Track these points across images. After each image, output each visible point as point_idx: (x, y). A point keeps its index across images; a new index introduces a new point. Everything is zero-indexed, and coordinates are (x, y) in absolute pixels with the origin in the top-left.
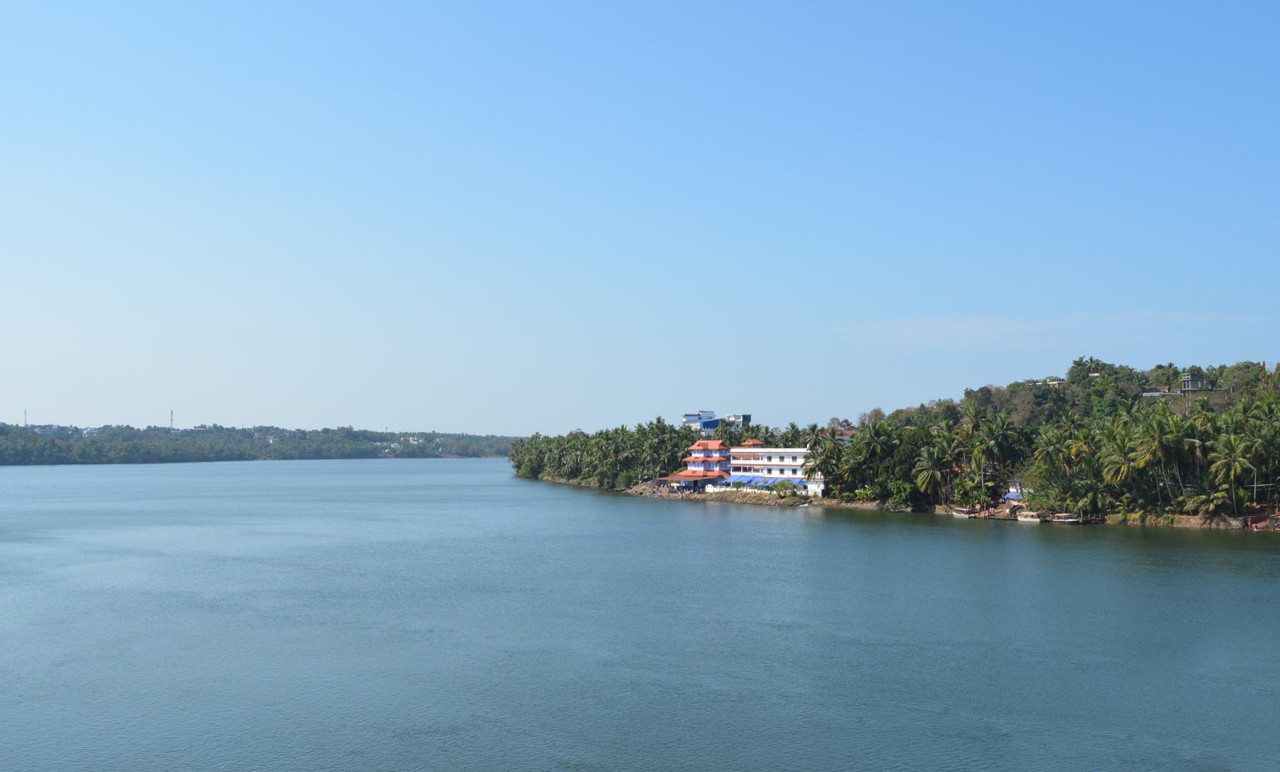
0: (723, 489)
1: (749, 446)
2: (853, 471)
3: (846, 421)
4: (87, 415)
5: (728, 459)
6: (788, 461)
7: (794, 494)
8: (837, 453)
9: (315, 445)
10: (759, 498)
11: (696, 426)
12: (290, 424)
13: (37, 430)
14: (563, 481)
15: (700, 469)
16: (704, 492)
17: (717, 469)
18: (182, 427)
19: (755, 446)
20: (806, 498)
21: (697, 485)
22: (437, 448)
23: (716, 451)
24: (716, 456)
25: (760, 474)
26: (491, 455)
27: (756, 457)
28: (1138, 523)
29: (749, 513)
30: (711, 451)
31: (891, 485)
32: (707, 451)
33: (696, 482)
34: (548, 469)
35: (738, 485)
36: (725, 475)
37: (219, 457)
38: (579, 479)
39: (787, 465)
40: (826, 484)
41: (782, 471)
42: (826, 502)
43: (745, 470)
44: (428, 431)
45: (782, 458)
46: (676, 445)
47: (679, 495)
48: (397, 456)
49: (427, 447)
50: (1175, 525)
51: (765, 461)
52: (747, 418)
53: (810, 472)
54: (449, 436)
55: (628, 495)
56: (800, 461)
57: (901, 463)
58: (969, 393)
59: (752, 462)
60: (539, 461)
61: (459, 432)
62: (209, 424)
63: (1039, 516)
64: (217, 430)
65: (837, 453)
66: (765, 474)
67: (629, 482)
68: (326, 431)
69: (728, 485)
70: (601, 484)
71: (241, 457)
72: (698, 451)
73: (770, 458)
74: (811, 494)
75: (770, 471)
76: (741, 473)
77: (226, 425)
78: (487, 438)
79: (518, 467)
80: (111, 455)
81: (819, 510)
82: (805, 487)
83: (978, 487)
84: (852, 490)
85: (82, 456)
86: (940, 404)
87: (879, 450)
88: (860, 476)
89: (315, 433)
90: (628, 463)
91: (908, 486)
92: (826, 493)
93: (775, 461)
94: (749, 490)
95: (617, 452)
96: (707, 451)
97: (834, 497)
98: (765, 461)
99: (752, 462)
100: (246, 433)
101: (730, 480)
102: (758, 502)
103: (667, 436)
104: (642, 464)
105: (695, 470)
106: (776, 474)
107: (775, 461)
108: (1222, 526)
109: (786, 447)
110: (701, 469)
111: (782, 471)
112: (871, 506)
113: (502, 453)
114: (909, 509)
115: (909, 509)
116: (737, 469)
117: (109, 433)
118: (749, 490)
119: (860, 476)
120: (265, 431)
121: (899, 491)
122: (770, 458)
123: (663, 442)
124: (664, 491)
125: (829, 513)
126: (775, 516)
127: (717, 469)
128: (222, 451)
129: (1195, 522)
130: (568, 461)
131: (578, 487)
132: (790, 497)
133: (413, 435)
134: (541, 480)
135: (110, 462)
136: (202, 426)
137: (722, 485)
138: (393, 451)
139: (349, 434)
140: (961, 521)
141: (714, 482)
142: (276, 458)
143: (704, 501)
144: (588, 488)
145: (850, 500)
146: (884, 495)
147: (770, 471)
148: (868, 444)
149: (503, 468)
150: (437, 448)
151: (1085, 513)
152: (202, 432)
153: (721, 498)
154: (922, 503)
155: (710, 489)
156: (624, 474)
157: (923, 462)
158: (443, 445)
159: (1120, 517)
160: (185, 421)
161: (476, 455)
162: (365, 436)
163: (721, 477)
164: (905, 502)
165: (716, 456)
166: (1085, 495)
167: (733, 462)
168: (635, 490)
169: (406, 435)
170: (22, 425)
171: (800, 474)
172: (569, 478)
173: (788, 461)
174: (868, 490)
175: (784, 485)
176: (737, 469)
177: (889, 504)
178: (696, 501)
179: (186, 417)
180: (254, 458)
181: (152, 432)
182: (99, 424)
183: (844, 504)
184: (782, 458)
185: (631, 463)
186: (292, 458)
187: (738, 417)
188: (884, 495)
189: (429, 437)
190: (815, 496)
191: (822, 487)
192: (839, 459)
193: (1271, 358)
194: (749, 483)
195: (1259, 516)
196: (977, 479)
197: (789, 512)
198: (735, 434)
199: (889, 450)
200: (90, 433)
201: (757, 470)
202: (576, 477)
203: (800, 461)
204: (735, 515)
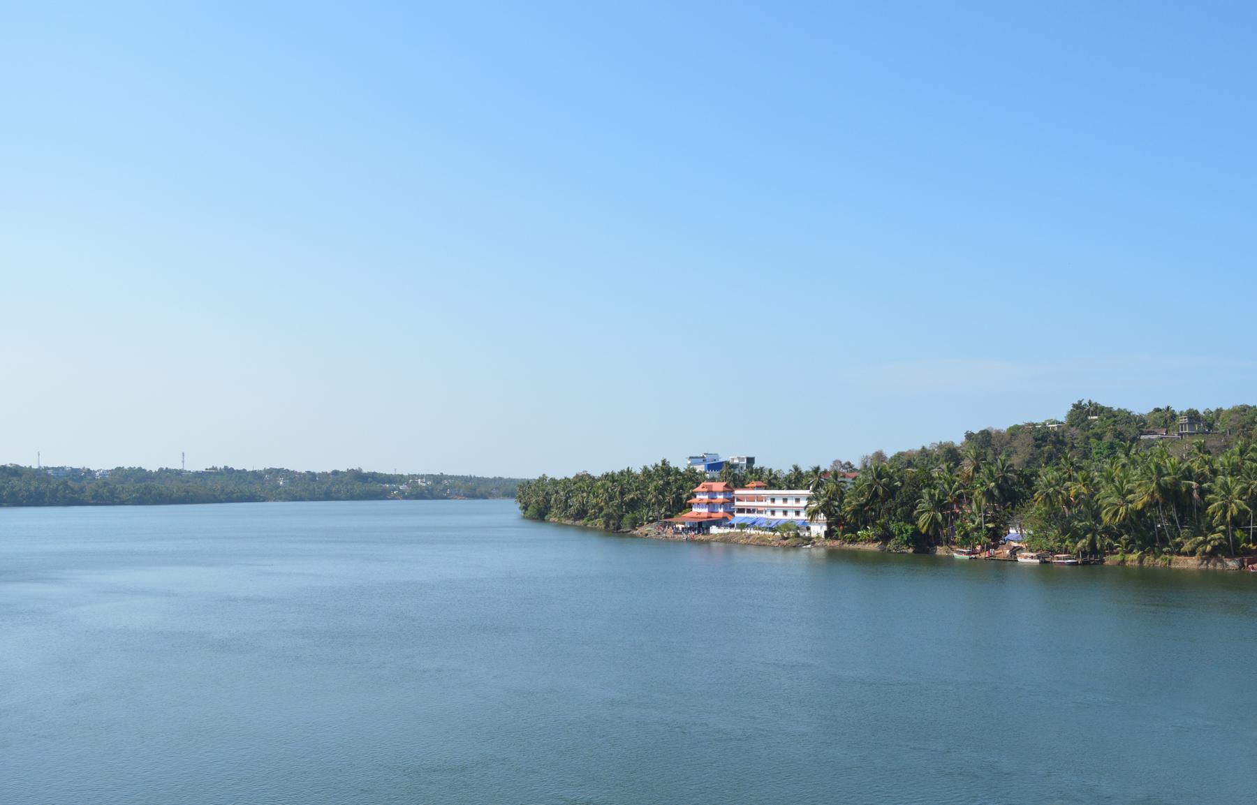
0: (727, 530)
1: (753, 488)
2: (855, 512)
3: (849, 463)
4: (100, 457)
5: (732, 501)
6: (791, 503)
7: (797, 535)
8: (839, 495)
10: (762, 539)
11: (700, 468)
12: (300, 464)
13: (50, 472)
14: (569, 522)
15: (705, 511)
16: (708, 533)
17: (721, 510)
19: (758, 487)
20: (810, 539)
21: (701, 526)
22: (445, 490)
23: (720, 493)
24: (720, 497)
25: (763, 515)
26: (498, 496)
27: (760, 499)
28: (1136, 564)
29: (753, 554)
31: (893, 527)
33: (700, 524)
34: (554, 510)
35: (742, 526)
36: (729, 516)
38: (585, 520)
39: (791, 506)
40: (829, 525)
41: (785, 513)
42: (829, 543)
43: (749, 511)
44: (436, 472)
45: (785, 500)
46: (681, 487)
47: (684, 537)
48: (406, 498)
49: (436, 489)
50: (1173, 566)
51: (769, 503)
52: (751, 461)
53: (813, 514)
54: (457, 478)
55: (633, 536)
56: (804, 503)
57: (902, 504)
58: (969, 436)
59: (756, 504)
60: (545, 502)
61: (466, 474)
62: (220, 466)
63: (1038, 557)
64: (228, 471)
65: (839, 495)
66: (768, 515)
67: (635, 524)
68: (335, 473)
69: (732, 526)
70: (607, 525)
71: (251, 498)
73: (773, 500)
75: (773, 512)
76: (745, 515)
78: (495, 480)
79: (525, 508)
80: (124, 496)
81: (822, 551)
82: (808, 529)
83: (978, 529)
84: (854, 532)
86: (941, 446)
87: (881, 491)
88: (862, 517)
89: (325, 475)
90: (633, 505)
91: (909, 527)
92: (829, 534)
93: (779, 503)
94: (753, 532)
95: (622, 494)
97: (837, 539)
101: (734, 521)
102: (762, 544)
103: (672, 478)
104: (648, 506)
105: (700, 512)
106: (779, 515)
107: (779, 503)
108: (1219, 566)
109: (789, 488)
110: (706, 510)
111: (785, 513)
112: (874, 547)
113: (509, 495)
114: (911, 550)
115: (911, 550)
116: (741, 510)
118: (753, 532)
119: (862, 517)
121: (901, 532)
122: (773, 500)
123: (668, 483)
124: (669, 532)
125: (832, 554)
126: (779, 557)
127: (721, 510)
128: (232, 493)
129: (1192, 563)
130: (575, 502)
131: (584, 529)
132: (794, 538)
133: (422, 477)
134: (548, 521)
135: (122, 503)
136: (214, 468)
139: (358, 476)
140: (962, 562)
141: (718, 523)
142: (286, 500)
143: (708, 542)
144: (594, 530)
145: (853, 541)
146: (886, 537)
147: (773, 512)
148: (870, 486)
149: (511, 509)
150: (445, 490)
151: (1084, 554)
152: (212, 474)
153: (726, 539)
154: (924, 544)
155: (714, 530)
156: (630, 515)
157: (924, 504)
158: (452, 487)
159: (1118, 558)
160: (196, 463)
161: (484, 496)
162: (373, 477)
163: (725, 519)
164: (907, 543)
165: (720, 497)
166: (1084, 537)
167: (737, 503)
168: (639, 531)
169: (414, 477)
170: (35, 467)
171: (803, 516)
172: (575, 520)
173: (791, 503)
174: (870, 532)
175: (787, 526)
176: (741, 510)
177: (891, 545)
178: (701, 542)
180: (264, 499)
181: (164, 474)
183: (846, 545)
184: (785, 500)
186: (301, 499)
188: (886, 537)
189: (438, 479)
190: (818, 537)
191: (825, 528)
192: (841, 501)
194: (753, 525)
196: (977, 521)
197: (792, 553)
198: (738, 476)
199: (891, 492)
200: (103, 475)
201: (761, 512)
202: (582, 518)
203: (804, 503)
204: (739, 556)
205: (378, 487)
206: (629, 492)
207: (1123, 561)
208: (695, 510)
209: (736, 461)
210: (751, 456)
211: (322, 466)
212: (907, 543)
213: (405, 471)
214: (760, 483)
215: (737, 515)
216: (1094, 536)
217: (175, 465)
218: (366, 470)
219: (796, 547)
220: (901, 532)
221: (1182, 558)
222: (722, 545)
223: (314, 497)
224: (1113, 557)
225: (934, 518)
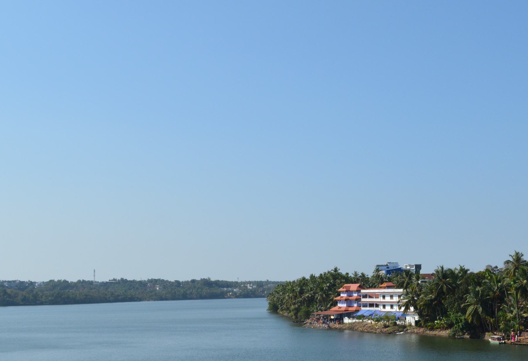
1: (384, 288)
4: (39, 274)
7: (395, 324)
9: (182, 291)
10: (372, 327)
11: (383, 273)
13: (6, 284)
19: (389, 287)
20: (404, 327)
30: (352, 292)
32: (348, 291)
37: (117, 299)
39: (389, 301)
48: (237, 297)
49: (61, 294)
56: (396, 299)
62: (119, 278)
64: (124, 281)
67: (308, 315)
68: (193, 281)
71: (132, 299)
72: (343, 292)
73: (384, 297)
74: (407, 323)
76: (368, 308)
77: (130, 278)
81: (414, 337)
83: (514, 318)
85: (23, 300)
89: (187, 283)
90: (311, 301)
93: (388, 299)
96: (348, 291)
98: (381, 299)
99: (374, 300)
100: (142, 284)
102: (371, 331)
105: (342, 306)
107: (388, 299)
112: (445, 333)
115: (468, 337)
117: (52, 285)
120: (154, 282)
121: (457, 322)
122: (384, 297)
128: (118, 296)
132: (392, 326)
133: (250, 283)
135: (42, 304)
136: (114, 280)
137: (353, 318)
138: (235, 293)
139: (207, 283)
140: (495, 346)
141: (350, 315)
142: (155, 300)
143: (341, 330)
145: (432, 329)
148: (437, 284)
150: (263, 291)
152: (114, 283)
153: (351, 327)
154: (477, 329)
155: (346, 320)
157: (470, 298)
160: (103, 276)
162: (218, 284)
169: (245, 283)
175: (387, 317)
180: (140, 300)
181: (82, 284)
182: (46, 280)
183: (428, 332)
185: (308, 301)
186: (166, 299)
187: (412, 266)
190: (410, 325)
196: (515, 312)
200: (40, 285)
203: (396, 299)
205: (218, 290)
206: (306, 292)
208: (339, 305)
209: (408, 268)
210: (418, 263)
211: (184, 277)
212: (462, 330)
213: (241, 279)
214: (390, 284)
215: (362, 308)
217: (89, 278)
218: (213, 278)
219: (392, 334)
220: (457, 322)
223: (174, 298)
225: (476, 311)
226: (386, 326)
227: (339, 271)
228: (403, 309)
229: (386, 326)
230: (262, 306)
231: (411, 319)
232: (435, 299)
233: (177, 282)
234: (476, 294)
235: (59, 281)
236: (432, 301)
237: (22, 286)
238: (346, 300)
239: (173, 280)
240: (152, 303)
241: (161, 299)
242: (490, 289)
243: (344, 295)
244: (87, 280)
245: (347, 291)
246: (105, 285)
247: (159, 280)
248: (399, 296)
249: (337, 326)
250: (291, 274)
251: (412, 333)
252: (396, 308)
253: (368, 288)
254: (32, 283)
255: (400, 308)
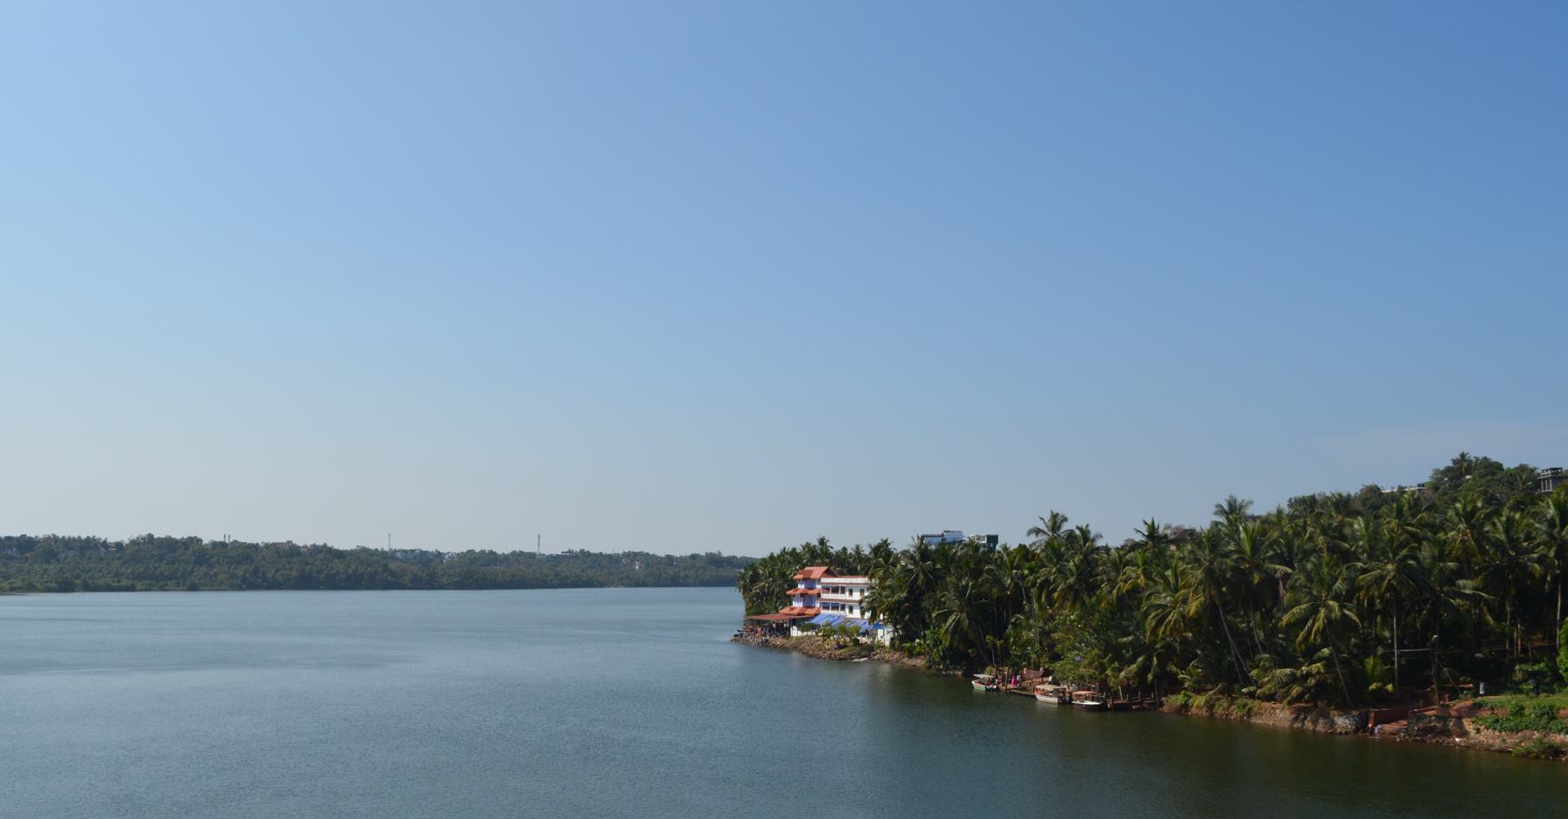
12: (660, 548)
18: (547, 553)
28: (1204, 712)
39: (847, 604)
43: (835, 607)
50: (1253, 720)
52: (993, 539)
63: (1056, 692)
64: (585, 554)
68: (694, 557)
71: (588, 584)
76: (830, 612)
80: (443, 580)
100: (613, 560)
108: (1321, 727)
120: (633, 556)
129: (1279, 716)
132: (850, 649)
135: (442, 587)
140: (979, 693)
142: (695, 585)
152: (570, 557)
155: (795, 632)
159: (1179, 699)
160: (552, 547)
166: (1132, 661)
179: (552, 538)
180: (602, 585)
181: (518, 556)
186: (645, 585)
193: (1565, 468)
195: (1392, 708)
203: (857, 596)
207: (1186, 706)
211: (681, 550)
216: (1149, 659)
221: (1257, 702)
222: (804, 658)
223: (659, 582)
224: (1173, 698)
225: (958, 623)
226: (840, 647)
227: (1100, 543)
228: (868, 615)
229: (840, 647)
230: (731, 605)
231: (885, 635)
232: (907, 599)
233: (670, 558)
234: (961, 592)
235: (483, 552)
236: (900, 602)
237: (289, 552)
238: (802, 595)
239: (662, 555)
240: (622, 589)
241: (637, 584)
242: (998, 581)
243: (801, 587)
244: (526, 550)
245: (805, 580)
246: (555, 560)
247: (641, 554)
248: (862, 591)
249: (779, 641)
250: (759, 547)
251: (882, 660)
252: (857, 613)
253: (842, 574)
254: (439, 555)
255: (863, 614)
